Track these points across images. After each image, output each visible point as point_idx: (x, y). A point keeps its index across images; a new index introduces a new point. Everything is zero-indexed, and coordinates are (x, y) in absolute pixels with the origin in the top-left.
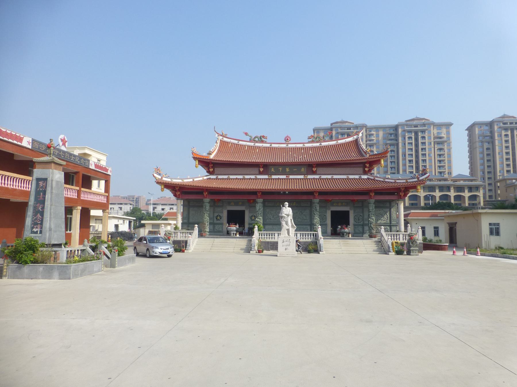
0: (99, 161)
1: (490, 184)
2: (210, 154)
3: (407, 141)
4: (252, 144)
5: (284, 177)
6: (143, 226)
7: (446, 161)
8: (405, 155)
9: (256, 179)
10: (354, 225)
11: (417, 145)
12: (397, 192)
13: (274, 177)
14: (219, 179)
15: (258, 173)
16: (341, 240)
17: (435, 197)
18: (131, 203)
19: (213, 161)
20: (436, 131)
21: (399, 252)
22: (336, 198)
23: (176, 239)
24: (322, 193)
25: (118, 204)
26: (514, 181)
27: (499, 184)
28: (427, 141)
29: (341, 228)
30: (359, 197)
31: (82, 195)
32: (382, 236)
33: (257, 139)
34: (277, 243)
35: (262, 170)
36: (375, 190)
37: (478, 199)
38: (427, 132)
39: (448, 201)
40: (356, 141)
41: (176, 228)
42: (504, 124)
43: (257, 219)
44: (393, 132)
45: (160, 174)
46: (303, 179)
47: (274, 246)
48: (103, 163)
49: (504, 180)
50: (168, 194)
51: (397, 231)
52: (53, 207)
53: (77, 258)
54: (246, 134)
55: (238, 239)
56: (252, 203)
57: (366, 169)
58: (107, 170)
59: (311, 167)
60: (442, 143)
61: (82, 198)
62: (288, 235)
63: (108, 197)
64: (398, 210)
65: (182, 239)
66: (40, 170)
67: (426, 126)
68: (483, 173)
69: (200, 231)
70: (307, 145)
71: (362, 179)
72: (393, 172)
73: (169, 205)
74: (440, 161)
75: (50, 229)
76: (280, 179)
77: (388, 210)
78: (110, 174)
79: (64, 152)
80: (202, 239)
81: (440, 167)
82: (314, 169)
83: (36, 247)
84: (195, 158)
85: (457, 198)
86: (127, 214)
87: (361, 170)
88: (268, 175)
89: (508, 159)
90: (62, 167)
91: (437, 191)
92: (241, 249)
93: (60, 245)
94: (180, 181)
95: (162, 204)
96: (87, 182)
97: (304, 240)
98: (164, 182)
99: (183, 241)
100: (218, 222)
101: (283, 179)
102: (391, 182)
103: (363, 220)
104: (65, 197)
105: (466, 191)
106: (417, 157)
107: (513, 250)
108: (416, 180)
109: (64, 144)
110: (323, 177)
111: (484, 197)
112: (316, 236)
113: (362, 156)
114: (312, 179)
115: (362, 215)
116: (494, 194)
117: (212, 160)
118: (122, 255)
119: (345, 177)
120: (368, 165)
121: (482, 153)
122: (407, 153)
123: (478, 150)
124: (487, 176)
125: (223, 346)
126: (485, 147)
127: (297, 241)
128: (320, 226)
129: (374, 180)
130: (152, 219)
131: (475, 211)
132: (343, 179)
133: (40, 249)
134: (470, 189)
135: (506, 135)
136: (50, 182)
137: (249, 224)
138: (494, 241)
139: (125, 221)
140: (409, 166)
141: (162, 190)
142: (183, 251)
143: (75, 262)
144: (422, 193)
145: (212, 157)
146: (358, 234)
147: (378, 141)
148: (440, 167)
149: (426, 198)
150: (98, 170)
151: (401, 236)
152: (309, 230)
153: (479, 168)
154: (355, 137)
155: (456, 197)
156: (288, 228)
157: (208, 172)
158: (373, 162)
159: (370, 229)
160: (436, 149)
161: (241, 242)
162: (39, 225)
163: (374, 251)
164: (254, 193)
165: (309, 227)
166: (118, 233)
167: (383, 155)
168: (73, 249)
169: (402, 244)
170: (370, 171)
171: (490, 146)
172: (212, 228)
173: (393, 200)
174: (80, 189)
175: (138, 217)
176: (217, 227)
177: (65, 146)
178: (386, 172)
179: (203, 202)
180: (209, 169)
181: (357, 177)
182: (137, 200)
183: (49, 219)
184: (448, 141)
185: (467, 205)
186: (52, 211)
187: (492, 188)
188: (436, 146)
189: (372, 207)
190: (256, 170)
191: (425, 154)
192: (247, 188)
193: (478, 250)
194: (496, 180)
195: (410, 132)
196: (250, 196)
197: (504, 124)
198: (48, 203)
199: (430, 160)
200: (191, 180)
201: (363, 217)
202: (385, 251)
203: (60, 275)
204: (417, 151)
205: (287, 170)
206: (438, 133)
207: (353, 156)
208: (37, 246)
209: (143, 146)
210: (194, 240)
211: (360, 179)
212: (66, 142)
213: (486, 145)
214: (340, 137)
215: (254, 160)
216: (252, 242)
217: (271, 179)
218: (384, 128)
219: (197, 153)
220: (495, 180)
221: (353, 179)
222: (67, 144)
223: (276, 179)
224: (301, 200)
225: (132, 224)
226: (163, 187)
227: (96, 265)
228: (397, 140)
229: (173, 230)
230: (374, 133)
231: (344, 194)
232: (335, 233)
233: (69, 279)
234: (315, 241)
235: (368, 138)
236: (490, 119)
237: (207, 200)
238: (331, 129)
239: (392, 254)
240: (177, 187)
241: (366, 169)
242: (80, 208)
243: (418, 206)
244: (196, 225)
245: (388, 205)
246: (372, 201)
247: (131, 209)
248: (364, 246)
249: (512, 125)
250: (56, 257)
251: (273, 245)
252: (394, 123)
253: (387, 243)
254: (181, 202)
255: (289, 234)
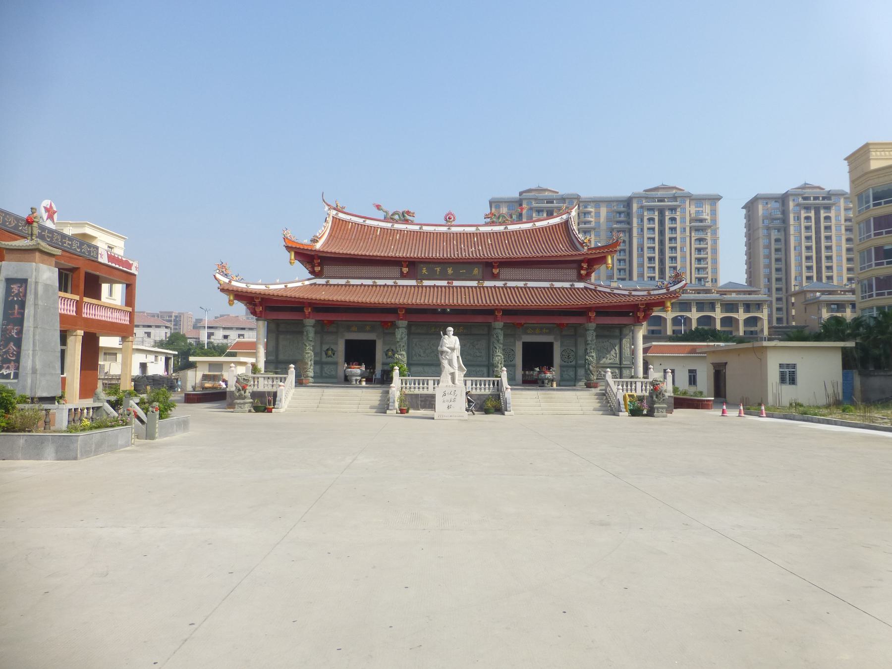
0: (111, 248)
1: (779, 299)
2: (315, 241)
3: (646, 225)
4: (389, 225)
5: (444, 283)
6: (192, 366)
7: (709, 261)
8: (642, 250)
9: (396, 286)
10: (561, 366)
11: (662, 233)
12: (635, 311)
13: (426, 283)
14: (331, 285)
15: (399, 275)
16: (540, 392)
17: (690, 319)
18: (168, 324)
19: (321, 254)
20: (693, 209)
21: (635, 412)
22: (532, 320)
23: (255, 389)
24: (508, 312)
25: (144, 326)
26: (818, 294)
27: (793, 300)
28: (678, 225)
29: (540, 372)
30: (570, 319)
31: (84, 310)
32: (608, 384)
33: (396, 217)
34: (433, 397)
35: (405, 270)
36: (597, 307)
37: (759, 324)
38: (679, 210)
39: (712, 327)
40: (566, 224)
41: (255, 369)
42: (805, 198)
43: (396, 356)
44: (624, 208)
45: (226, 275)
46: (476, 287)
47: (428, 402)
48: (119, 252)
49: (803, 292)
50: (240, 308)
51: (632, 377)
52: (38, 331)
53: (87, 422)
54: (378, 207)
55: (364, 390)
56: (388, 328)
57: (583, 272)
58: (130, 266)
59: (489, 267)
60: (702, 228)
61: (84, 316)
62: (453, 383)
63: (131, 315)
64: (633, 342)
65: (267, 389)
66: (14, 264)
67: (679, 199)
68: (769, 280)
69: (298, 376)
70: (483, 229)
71: (574, 289)
72: (622, 277)
73: (237, 329)
74: (699, 260)
75: (34, 371)
76: (438, 287)
77: (617, 341)
78: (136, 273)
79: (51, 231)
80: (302, 390)
81: (698, 269)
82: (496, 271)
83: (11, 403)
84: (289, 248)
85: (726, 321)
86: (161, 344)
87: (573, 273)
88: (417, 279)
89: (808, 258)
90: (53, 260)
91: (694, 309)
92: (372, 408)
93: (51, 400)
94: (263, 287)
95: (224, 328)
96: (92, 287)
97: (478, 392)
98: (235, 289)
99: (269, 393)
100: (329, 359)
101: (441, 287)
102: (624, 295)
103: (576, 358)
104: (61, 316)
105: (741, 310)
106: (662, 252)
107: (819, 407)
108: (664, 291)
109: (50, 217)
110: (511, 284)
111: (770, 322)
112: (498, 385)
113: (576, 249)
114: (491, 287)
115: (574, 349)
116: (784, 316)
117: (319, 251)
118: (167, 417)
119: (546, 284)
120: (585, 266)
121: (768, 247)
122: (646, 245)
123: (762, 242)
124: (774, 286)
125: (374, 567)
126: (773, 238)
127: (467, 393)
128: (504, 369)
129: (595, 291)
130: (206, 354)
131: (757, 344)
132: (544, 288)
133: (19, 406)
134: (748, 307)
135: (808, 218)
136: (33, 286)
137: (383, 364)
138: (788, 394)
139: (159, 358)
140: (670, 267)
141: (231, 303)
142: (270, 411)
143: (84, 430)
144: (669, 315)
145: (318, 246)
146: (568, 382)
147: (598, 223)
148: (698, 269)
149: (676, 321)
150: (113, 265)
151: (639, 385)
152: (486, 374)
153: (762, 272)
154: (565, 217)
155: (724, 321)
156: (452, 371)
157: (312, 272)
158: (593, 261)
159: (588, 372)
160: (693, 239)
161: (373, 395)
162: (12, 364)
163: (595, 410)
164: (489, 312)
165: (485, 370)
166: (148, 378)
167: (611, 248)
168: (73, 407)
169: (641, 399)
170: (588, 275)
171: (781, 236)
172: (318, 370)
173: (626, 325)
174: (81, 299)
175: (182, 351)
176: (327, 369)
177: (53, 220)
178: (610, 277)
179: (304, 326)
180: (313, 267)
181: (567, 285)
182: (177, 321)
183: (31, 352)
184: (713, 227)
185: (741, 333)
186: (37, 337)
187: (783, 305)
188: (693, 234)
189: (591, 336)
190: (395, 271)
191: (675, 248)
192: (380, 301)
193: (763, 408)
194: (789, 293)
195: (651, 209)
196: (384, 316)
197: (805, 198)
198: (28, 324)
199: (684, 258)
200: (282, 286)
201: (576, 353)
202: (612, 410)
203: (57, 452)
204: (662, 243)
205: (450, 271)
206: (697, 212)
207: (561, 250)
208: (13, 400)
209: (199, 226)
210: (288, 392)
211: (572, 288)
212: (55, 212)
213: (774, 235)
214: (534, 215)
215: (391, 254)
216: (391, 396)
217: (422, 286)
218: (608, 202)
219: (293, 239)
220: (787, 291)
221: (557, 288)
222: (55, 216)
223: (430, 287)
224: (473, 322)
225: (172, 362)
226: (232, 298)
227: (121, 434)
228: (629, 223)
229: (250, 374)
230: (592, 210)
231: (544, 312)
232: (530, 382)
233: (75, 458)
234: (496, 393)
235: (582, 219)
236: (781, 190)
237: (310, 322)
238: (520, 203)
239: (624, 414)
240: (257, 298)
241: (583, 272)
242: (81, 333)
243: (662, 335)
244: (292, 366)
245: (617, 332)
246: (592, 326)
247: (168, 335)
248: (578, 402)
249: (817, 201)
250: (48, 420)
251: (425, 401)
252: (626, 193)
253: (616, 396)
254: (262, 326)
255: (453, 382)
